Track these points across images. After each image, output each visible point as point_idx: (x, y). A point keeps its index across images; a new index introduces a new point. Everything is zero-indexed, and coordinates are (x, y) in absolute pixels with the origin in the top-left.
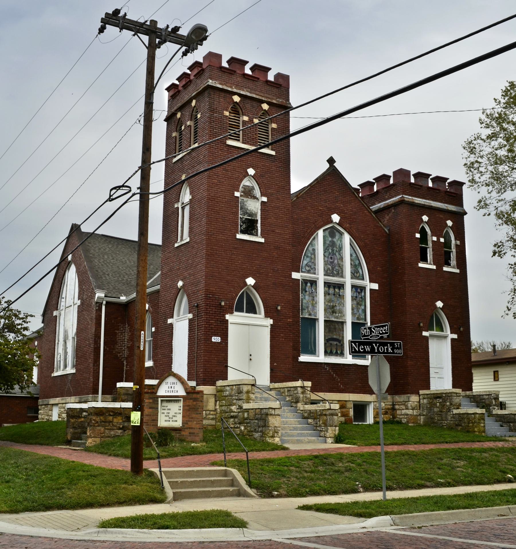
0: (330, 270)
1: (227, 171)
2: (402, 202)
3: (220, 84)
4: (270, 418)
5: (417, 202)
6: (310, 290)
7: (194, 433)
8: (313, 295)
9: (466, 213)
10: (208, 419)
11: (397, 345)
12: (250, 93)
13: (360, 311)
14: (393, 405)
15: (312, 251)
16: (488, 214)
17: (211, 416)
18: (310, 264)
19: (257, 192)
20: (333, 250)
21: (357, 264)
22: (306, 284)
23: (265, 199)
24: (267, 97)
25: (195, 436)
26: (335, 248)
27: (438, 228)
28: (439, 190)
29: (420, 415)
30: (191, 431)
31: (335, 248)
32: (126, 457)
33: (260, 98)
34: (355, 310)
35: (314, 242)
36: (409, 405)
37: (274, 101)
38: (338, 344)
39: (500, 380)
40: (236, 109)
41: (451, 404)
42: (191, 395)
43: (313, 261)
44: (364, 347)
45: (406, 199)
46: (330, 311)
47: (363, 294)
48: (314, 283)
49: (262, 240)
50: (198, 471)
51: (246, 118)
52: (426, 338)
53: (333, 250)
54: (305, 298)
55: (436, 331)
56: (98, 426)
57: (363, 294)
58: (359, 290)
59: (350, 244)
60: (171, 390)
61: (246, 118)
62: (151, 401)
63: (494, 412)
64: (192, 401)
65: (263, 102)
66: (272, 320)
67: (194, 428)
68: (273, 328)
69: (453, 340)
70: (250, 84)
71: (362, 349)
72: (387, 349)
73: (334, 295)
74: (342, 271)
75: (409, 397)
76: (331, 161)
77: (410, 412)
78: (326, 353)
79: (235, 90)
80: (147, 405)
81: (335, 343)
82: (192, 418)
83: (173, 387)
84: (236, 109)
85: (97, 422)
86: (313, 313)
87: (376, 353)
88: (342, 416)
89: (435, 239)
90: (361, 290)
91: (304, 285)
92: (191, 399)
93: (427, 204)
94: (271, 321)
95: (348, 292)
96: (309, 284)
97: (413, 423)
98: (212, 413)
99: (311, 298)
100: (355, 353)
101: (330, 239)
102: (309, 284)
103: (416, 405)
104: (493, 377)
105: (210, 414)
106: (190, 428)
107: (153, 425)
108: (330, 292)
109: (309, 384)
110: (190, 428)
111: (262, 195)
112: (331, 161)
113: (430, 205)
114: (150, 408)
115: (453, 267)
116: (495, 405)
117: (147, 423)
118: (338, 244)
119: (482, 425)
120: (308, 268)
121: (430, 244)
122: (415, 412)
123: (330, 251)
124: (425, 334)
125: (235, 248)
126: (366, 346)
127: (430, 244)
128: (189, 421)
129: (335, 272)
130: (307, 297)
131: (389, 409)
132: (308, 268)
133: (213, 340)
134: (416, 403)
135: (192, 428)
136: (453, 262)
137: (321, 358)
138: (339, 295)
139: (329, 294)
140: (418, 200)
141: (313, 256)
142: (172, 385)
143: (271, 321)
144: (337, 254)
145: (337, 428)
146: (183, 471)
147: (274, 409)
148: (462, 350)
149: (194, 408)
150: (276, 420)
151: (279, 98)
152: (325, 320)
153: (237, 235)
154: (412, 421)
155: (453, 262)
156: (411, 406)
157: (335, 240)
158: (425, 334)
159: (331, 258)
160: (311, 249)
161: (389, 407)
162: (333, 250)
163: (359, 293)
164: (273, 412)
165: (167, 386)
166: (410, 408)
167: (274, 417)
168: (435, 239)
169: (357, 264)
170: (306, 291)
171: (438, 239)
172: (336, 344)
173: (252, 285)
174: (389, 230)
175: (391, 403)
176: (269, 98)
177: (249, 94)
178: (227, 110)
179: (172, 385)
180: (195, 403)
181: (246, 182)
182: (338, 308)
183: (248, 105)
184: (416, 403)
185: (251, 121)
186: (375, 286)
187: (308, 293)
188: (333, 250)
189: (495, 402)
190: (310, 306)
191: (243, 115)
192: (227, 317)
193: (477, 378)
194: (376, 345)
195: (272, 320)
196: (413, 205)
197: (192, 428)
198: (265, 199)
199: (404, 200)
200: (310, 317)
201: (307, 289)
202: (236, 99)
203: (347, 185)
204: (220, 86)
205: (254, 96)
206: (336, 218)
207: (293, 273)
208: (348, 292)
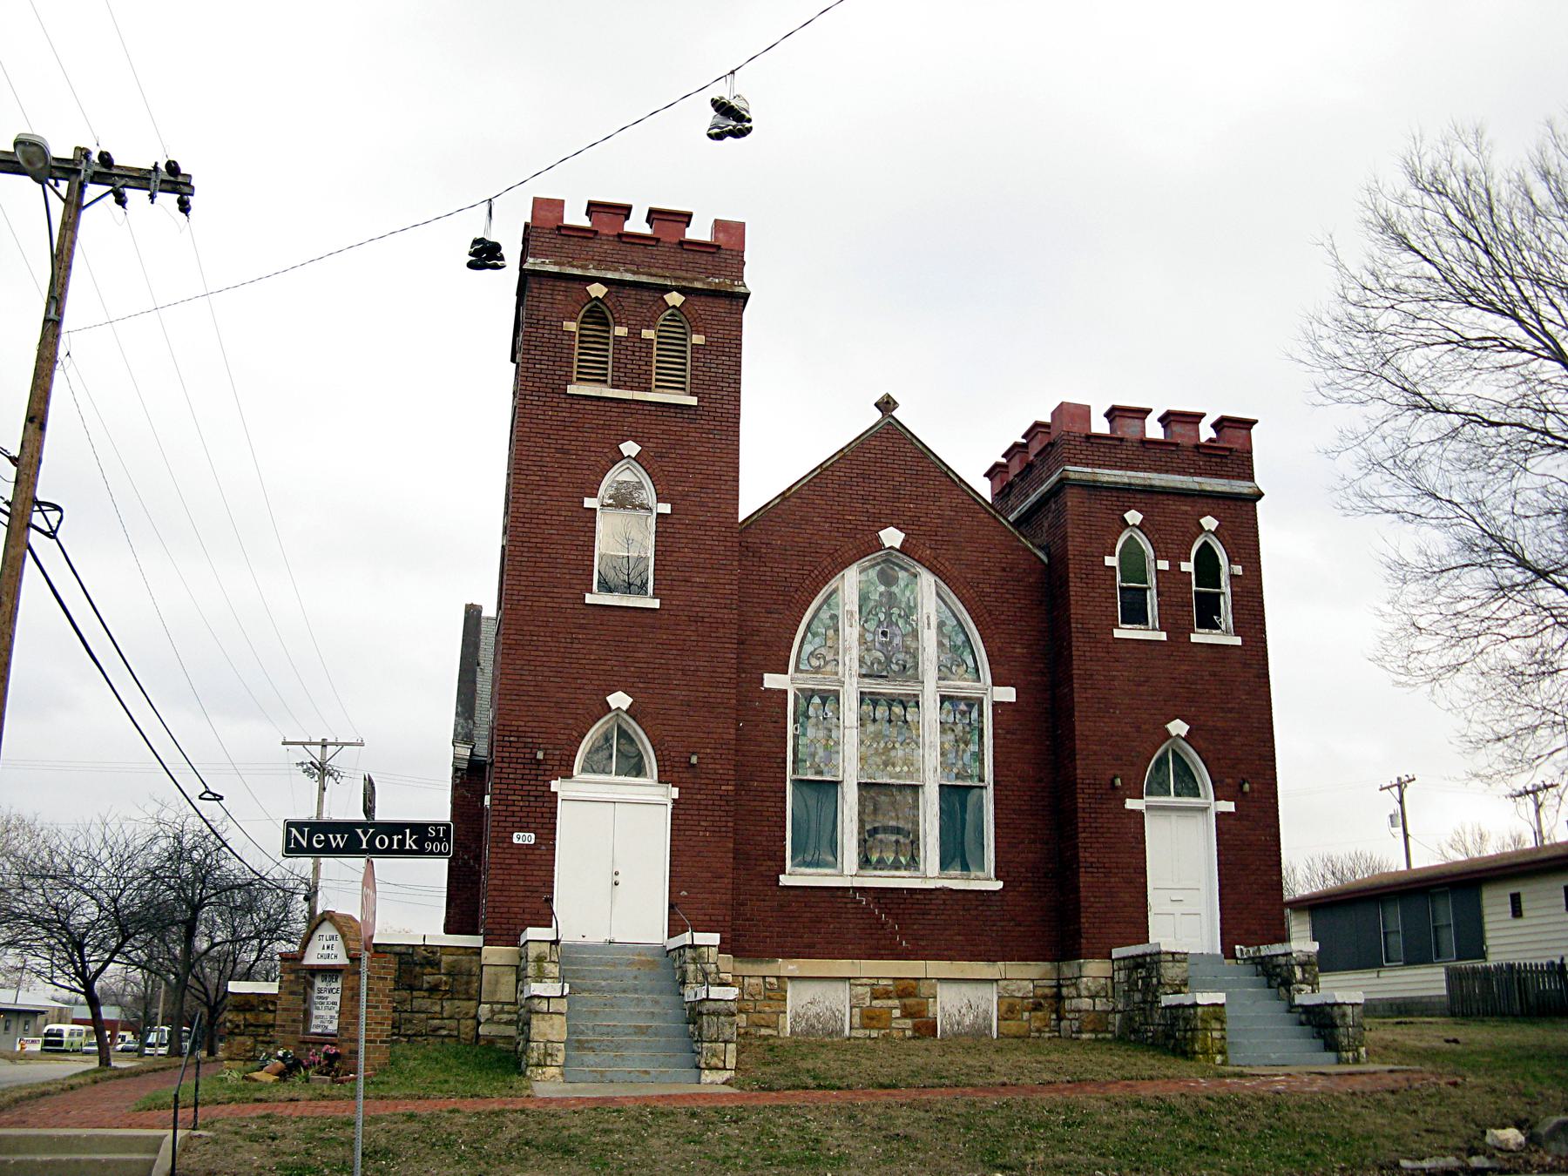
0: (879, 662)
1: (566, 452)
2: (1063, 483)
3: (555, 264)
4: (535, 1021)
5: (1106, 479)
6: (820, 712)
8: (830, 728)
9: (1260, 495)
10: (498, 1023)
11: (438, 832)
12: (634, 273)
13: (967, 757)
14: (1059, 986)
15: (828, 622)
17: (505, 1017)
18: (823, 651)
19: (649, 494)
20: (887, 616)
21: (959, 642)
23: (666, 508)
24: (676, 278)
26: (895, 610)
27: (1171, 542)
28: (1177, 445)
29: (1114, 1011)
31: (895, 610)
33: (660, 281)
34: (951, 756)
35: (832, 601)
37: (698, 285)
38: (902, 839)
40: (598, 315)
41: (1159, 982)
43: (829, 643)
44: (327, 839)
45: (1072, 475)
46: (878, 760)
47: (975, 714)
48: (830, 697)
49: (656, 604)
50: (90, 1138)
51: (621, 331)
52: (1138, 816)
53: (887, 616)
55: (1178, 794)
57: (975, 714)
58: (963, 707)
59: (938, 594)
61: (621, 331)
63: (1298, 1000)
66: (676, 790)
68: (679, 810)
69: (1220, 816)
71: (319, 842)
72: (402, 842)
73: (890, 721)
74: (916, 667)
75: (1080, 967)
76: (887, 405)
77: (1086, 1003)
78: (944, 864)
79: (593, 273)
81: (894, 838)
84: (598, 315)
86: (826, 770)
87: (364, 852)
88: (904, 1016)
89: (1164, 565)
90: (970, 706)
91: (802, 701)
93: (1138, 482)
94: (675, 793)
95: (930, 713)
96: (816, 700)
97: (1092, 1031)
98: (507, 1008)
99: (821, 734)
101: (882, 588)
102: (816, 700)
103: (1104, 987)
104: (1509, 907)
105: (502, 1011)
109: (714, 939)
111: (661, 499)
112: (887, 405)
113: (1147, 482)
115: (1227, 632)
116: (1301, 982)
118: (904, 600)
119: (1216, 1034)
120: (815, 662)
121: (1152, 581)
122: (1100, 1005)
123: (882, 617)
124: (1130, 804)
125: (582, 626)
126: (334, 833)
127: (1152, 581)
129: (894, 667)
130: (811, 732)
131: (1045, 997)
132: (815, 662)
133: (515, 841)
134: (1103, 981)
136: (1226, 616)
137: (847, 872)
138: (906, 722)
139: (874, 720)
140: (1108, 475)
143: (675, 793)
144: (901, 622)
145: (732, 1047)
146: (50, 1137)
151: (713, 275)
152: (941, 786)
153: (588, 595)
155: (1226, 616)
156: (1088, 989)
157: (894, 589)
158: (1130, 804)
159: (884, 634)
160: (825, 615)
161: (1047, 991)
162: (889, 615)
163: (963, 713)
164: (544, 1006)
166: (1084, 993)
168: (1164, 565)
169: (959, 642)
170: (808, 717)
171: (1175, 566)
172: (897, 842)
174: (1048, 555)
175: (1053, 983)
176: (685, 279)
177: (629, 277)
178: (572, 319)
181: (620, 475)
182: (900, 753)
183: (630, 300)
184: (1103, 981)
185: (635, 334)
186: (1008, 694)
187: (813, 720)
188: (889, 615)
189: (1304, 972)
190: (821, 752)
192: (555, 785)
193: (1493, 918)
195: (676, 790)
196: (1093, 487)
198: (666, 508)
201: (811, 712)
202: (597, 290)
203: (927, 457)
204: (555, 269)
205: (644, 279)
208: (930, 713)
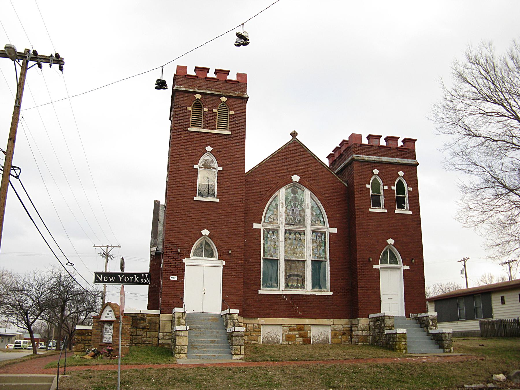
0: (292, 220)
2: (353, 160)
3: (184, 87)
4: (177, 339)
8: (275, 241)
9: (418, 164)
10: (165, 339)
11: (145, 276)
13: (321, 251)
14: (351, 327)
15: (275, 206)
17: (168, 337)
18: (273, 216)
19: (215, 164)
20: (294, 204)
22: (268, 232)
23: (221, 169)
24: (224, 92)
27: (388, 180)
28: (390, 147)
29: (369, 335)
33: (219, 93)
34: (316, 251)
36: (359, 327)
37: (231, 95)
38: (299, 278)
39: (506, 303)
40: (198, 105)
41: (384, 326)
43: (275, 213)
44: (109, 278)
45: (356, 158)
46: (291, 252)
47: (323, 237)
48: (275, 231)
49: (218, 200)
51: (206, 110)
52: (378, 271)
53: (294, 204)
54: (267, 244)
55: (390, 263)
56: (80, 343)
57: (323, 237)
58: (319, 234)
59: (311, 197)
61: (206, 110)
65: (221, 96)
66: (224, 262)
68: (225, 269)
69: (405, 271)
70: (212, 84)
71: (106, 279)
72: (133, 279)
73: (295, 239)
74: (304, 221)
75: (358, 321)
76: (294, 134)
77: (360, 333)
78: (313, 287)
79: (197, 90)
84: (198, 105)
85: (79, 340)
88: (300, 337)
89: (386, 187)
90: (322, 234)
91: (266, 232)
93: (377, 160)
94: (224, 263)
95: (309, 237)
96: (271, 232)
97: (362, 342)
98: (168, 334)
99: (272, 243)
101: (293, 195)
102: (271, 232)
103: (366, 328)
104: (501, 301)
105: (166, 335)
108: (291, 237)
109: (237, 311)
111: (219, 165)
112: (294, 134)
113: (381, 160)
115: (407, 210)
116: (432, 326)
118: (300, 199)
119: (403, 343)
120: (270, 220)
121: (382, 193)
122: (365, 333)
123: (293, 205)
124: (375, 267)
126: (111, 276)
127: (382, 193)
129: (297, 221)
130: (269, 243)
131: (347, 331)
132: (270, 220)
133: (171, 279)
134: (366, 325)
136: (407, 204)
137: (281, 289)
138: (300, 239)
139: (290, 239)
140: (367, 158)
141: (275, 210)
143: (224, 263)
144: (299, 206)
145: (243, 347)
147: (182, 331)
148: (414, 282)
150: (183, 340)
153: (195, 197)
154: (361, 341)
155: (407, 204)
157: (297, 195)
158: (375, 267)
159: (293, 210)
160: (273, 204)
161: (347, 329)
162: (295, 204)
163: (319, 237)
164: (180, 334)
166: (360, 329)
167: (181, 337)
168: (386, 187)
170: (268, 238)
171: (390, 188)
172: (298, 279)
173: (207, 235)
175: (349, 326)
176: (227, 93)
177: (208, 92)
178: (190, 106)
181: (206, 157)
182: (299, 250)
183: (209, 99)
184: (366, 325)
185: (210, 111)
187: (270, 239)
188: (295, 204)
189: (432, 322)
190: (272, 250)
191: (204, 107)
192: (184, 260)
193: (495, 304)
194: (121, 277)
195: (224, 262)
196: (363, 162)
198: (221, 169)
199: (354, 159)
200: (271, 258)
201: (269, 236)
202: (198, 96)
203: (307, 152)
204: (184, 89)
205: (214, 92)
206: (296, 178)
207: (254, 224)
208: (309, 237)
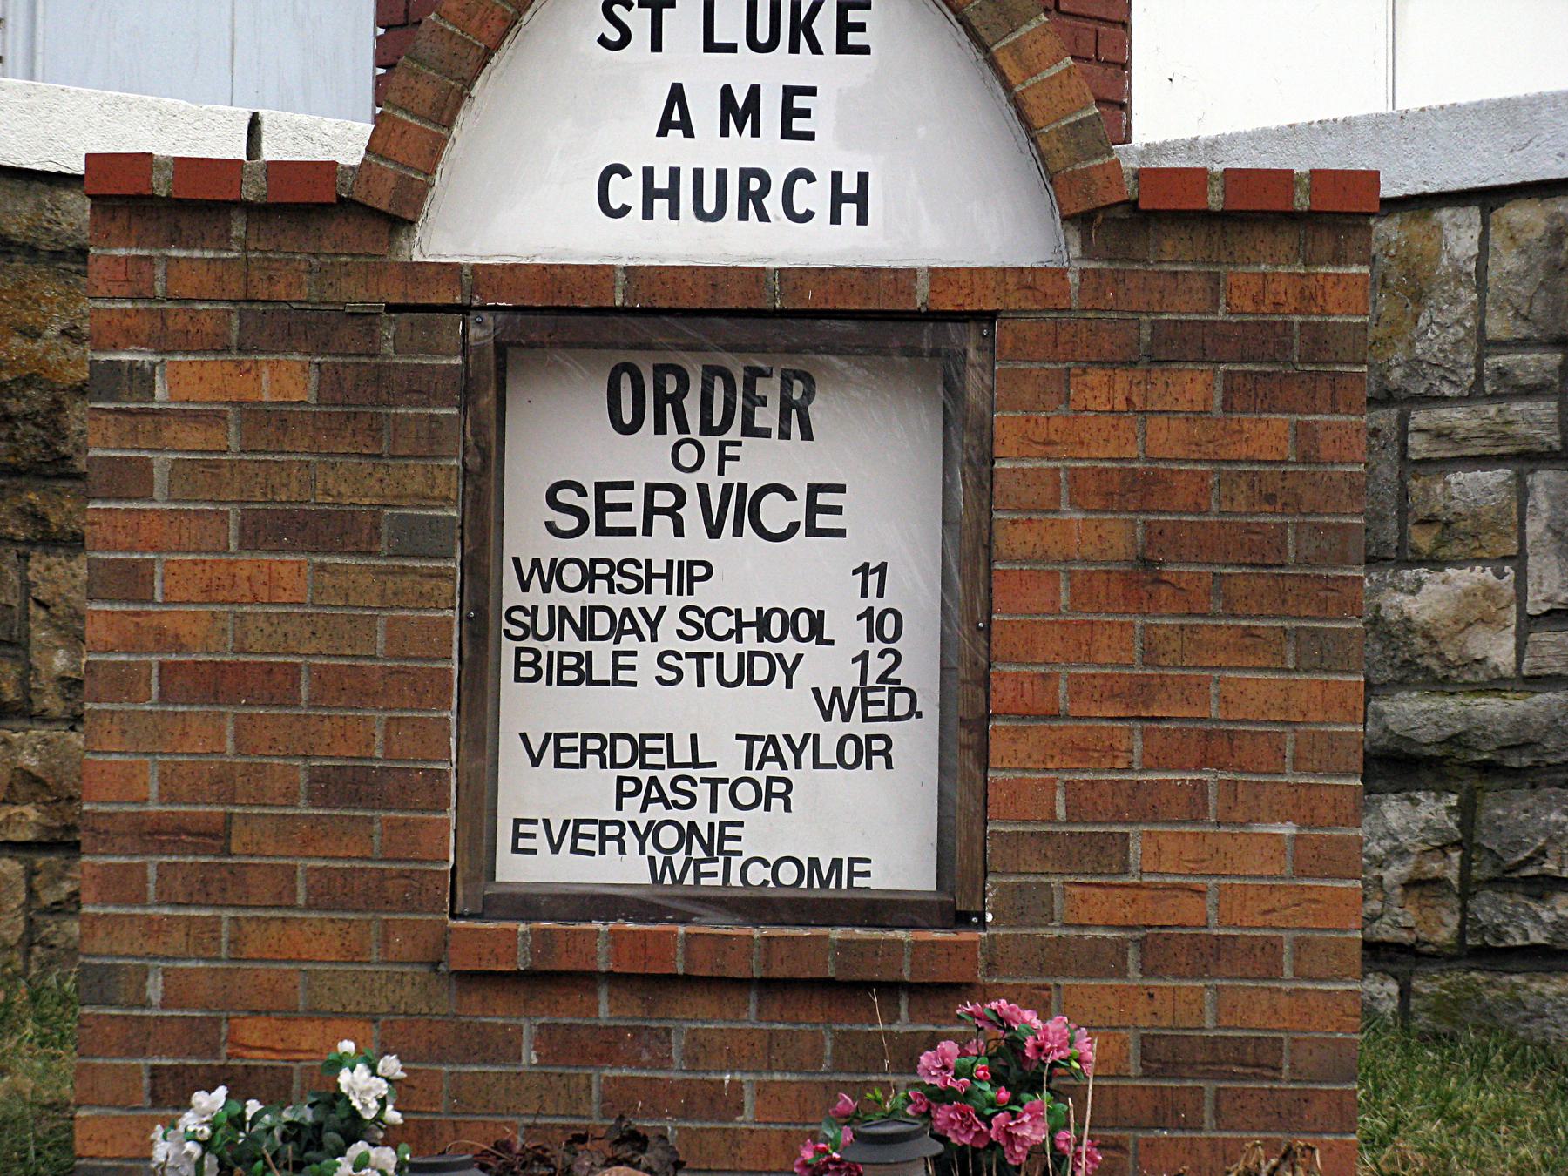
7: (1258, 1057)
16: (662, 1144)
25: (1286, 1114)
30: (1200, 1005)
32: (767, 965)
42: (1175, 255)
60: (739, 152)
62: (286, 378)
64: (1195, 386)
67: (1261, 958)
80: (199, 474)
82: (1215, 745)
83: (705, 110)
92: (1171, 347)
100: (313, 801)
106: (1160, 949)
107: (330, 894)
110: (1160, 949)
114: (270, 529)
117: (216, 836)
128: (1145, 805)
135: (1209, 954)
142: (743, 70)
149: (1262, 554)
165: (644, 76)
179: (743, 70)
180: (1269, 433)
197: (1209, 954)
